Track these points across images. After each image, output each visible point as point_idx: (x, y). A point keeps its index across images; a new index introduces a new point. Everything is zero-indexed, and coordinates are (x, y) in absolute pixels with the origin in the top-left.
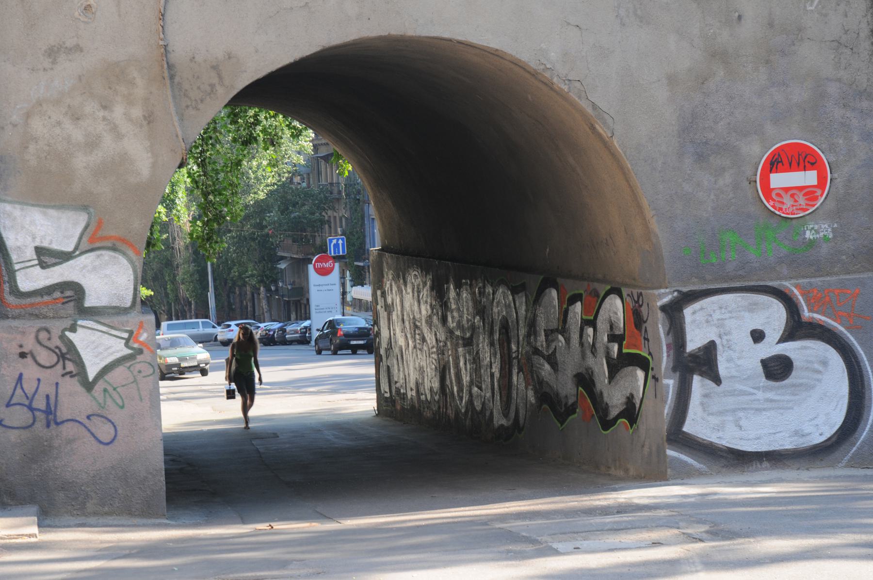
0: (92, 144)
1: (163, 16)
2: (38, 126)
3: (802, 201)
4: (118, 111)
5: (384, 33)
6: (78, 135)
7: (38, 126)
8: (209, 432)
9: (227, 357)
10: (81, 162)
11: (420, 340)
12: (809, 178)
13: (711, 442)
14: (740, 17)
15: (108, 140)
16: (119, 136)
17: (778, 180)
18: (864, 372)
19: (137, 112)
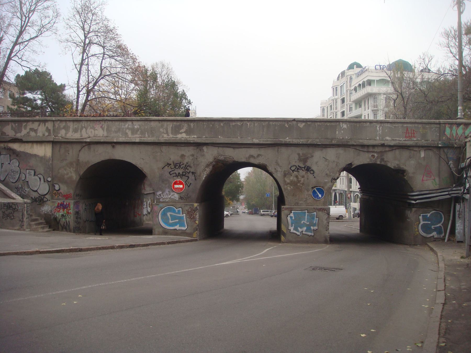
0: (67, 174)
1: (78, 155)
2: (60, 171)
3: (180, 190)
4: (72, 169)
5: (121, 159)
6: (66, 172)
7: (60, 171)
8: (347, 183)
9: (244, 188)
10: (66, 177)
11: (453, 164)
12: (181, 186)
13: (101, 236)
14: (170, 159)
15: (70, 174)
16: (71, 173)
17: (176, 186)
18: (276, 204)
19: (74, 169)
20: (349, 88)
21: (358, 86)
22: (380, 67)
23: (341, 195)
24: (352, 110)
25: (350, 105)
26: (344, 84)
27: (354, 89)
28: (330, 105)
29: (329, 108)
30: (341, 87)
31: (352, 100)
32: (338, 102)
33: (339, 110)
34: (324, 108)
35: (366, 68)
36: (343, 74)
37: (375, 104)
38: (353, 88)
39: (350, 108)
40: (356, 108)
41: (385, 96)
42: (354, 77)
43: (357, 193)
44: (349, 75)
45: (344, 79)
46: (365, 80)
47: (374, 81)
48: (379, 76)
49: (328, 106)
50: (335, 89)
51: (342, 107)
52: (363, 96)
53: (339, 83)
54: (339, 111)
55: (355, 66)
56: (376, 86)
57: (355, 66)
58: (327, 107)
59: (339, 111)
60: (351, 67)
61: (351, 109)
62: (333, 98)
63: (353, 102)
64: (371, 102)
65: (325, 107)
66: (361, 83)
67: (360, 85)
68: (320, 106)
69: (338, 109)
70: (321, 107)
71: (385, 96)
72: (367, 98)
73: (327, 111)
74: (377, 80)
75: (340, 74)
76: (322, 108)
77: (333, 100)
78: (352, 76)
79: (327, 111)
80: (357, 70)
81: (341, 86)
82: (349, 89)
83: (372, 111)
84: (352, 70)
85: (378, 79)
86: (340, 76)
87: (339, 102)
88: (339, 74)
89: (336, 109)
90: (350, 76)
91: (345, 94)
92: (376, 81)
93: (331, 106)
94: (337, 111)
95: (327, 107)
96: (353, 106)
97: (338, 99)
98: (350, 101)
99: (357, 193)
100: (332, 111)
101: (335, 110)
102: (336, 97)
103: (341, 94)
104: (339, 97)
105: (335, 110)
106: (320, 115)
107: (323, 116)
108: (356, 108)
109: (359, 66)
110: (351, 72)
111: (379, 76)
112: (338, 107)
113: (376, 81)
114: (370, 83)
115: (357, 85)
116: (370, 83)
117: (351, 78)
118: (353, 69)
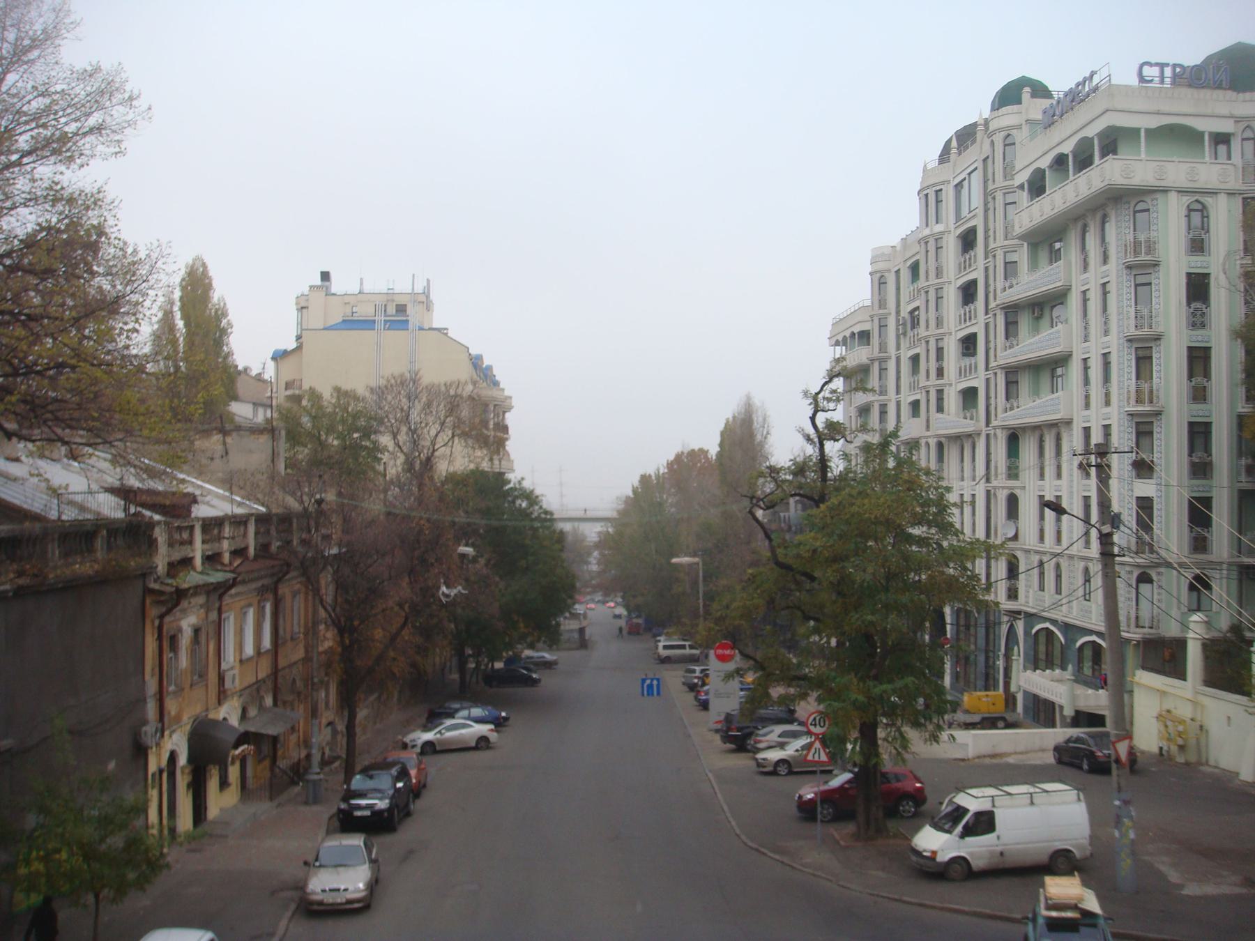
20: (1000, 181)
21: (1050, 167)
22: (1162, 72)
23: (962, 615)
24: (1015, 274)
25: (1005, 253)
26: (969, 174)
27: (1029, 182)
28: (909, 263)
29: (906, 275)
30: (959, 186)
31: (1018, 230)
32: (945, 299)
33: (952, 277)
34: (886, 274)
35: (1096, 80)
36: (966, 136)
37: (1142, 237)
38: (1023, 177)
39: (1006, 263)
40: (1034, 265)
41: (1186, 200)
42: (1020, 136)
43: (1047, 625)
44: (999, 130)
45: (974, 155)
46: (1092, 131)
47: (1133, 133)
48: (1158, 113)
49: (900, 266)
50: (931, 198)
51: (964, 267)
52: (1078, 206)
53: (952, 174)
54: (951, 385)
55: (1027, 89)
56: (1143, 156)
57: (1027, 89)
58: (898, 272)
59: (950, 282)
60: (1009, 95)
61: (1010, 269)
62: (927, 232)
63: (1023, 237)
64: (1118, 232)
65: (889, 271)
66: (1067, 148)
67: (1060, 161)
68: (869, 269)
69: (945, 324)
70: (871, 274)
71: (1186, 200)
72: (1080, 224)
73: (898, 289)
74: (1148, 131)
75: (954, 139)
76: (878, 275)
77: (924, 241)
78: (1014, 132)
79: (898, 289)
80: (1034, 108)
81: (956, 186)
82: (1001, 188)
83: (1129, 267)
84: (1015, 108)
85: (1154, 122)
86: (954, 144)
87: (951, 246)
88: (949, 142)
89: (939, 273)
90: (1003, 134)
91: (980, 212)
92: (1143, 134)
93: (915, 269)
94: (944, 334)
95: (898, 272)
96: (1022, 256)
97: (945, 287)
98: (1006, 238)
99: (1047, 625)
100: (922, 283)
101: (933, 280)
102: (939, 228)
103: (958, 217)
104: (952, 227)
105: (933, 280)
106: (868, 303)
107: (880, 308)
108: (1034, 265)
109: (1040, 91)
110: (1010, 117)
111: (1158, 113)
112: (945, 314)
113: (1143, 134)
114: (1112, 141)
115: (1045, 163)
116: (1112, 141)
117: (1009, 143)
118: (1020, 103)
